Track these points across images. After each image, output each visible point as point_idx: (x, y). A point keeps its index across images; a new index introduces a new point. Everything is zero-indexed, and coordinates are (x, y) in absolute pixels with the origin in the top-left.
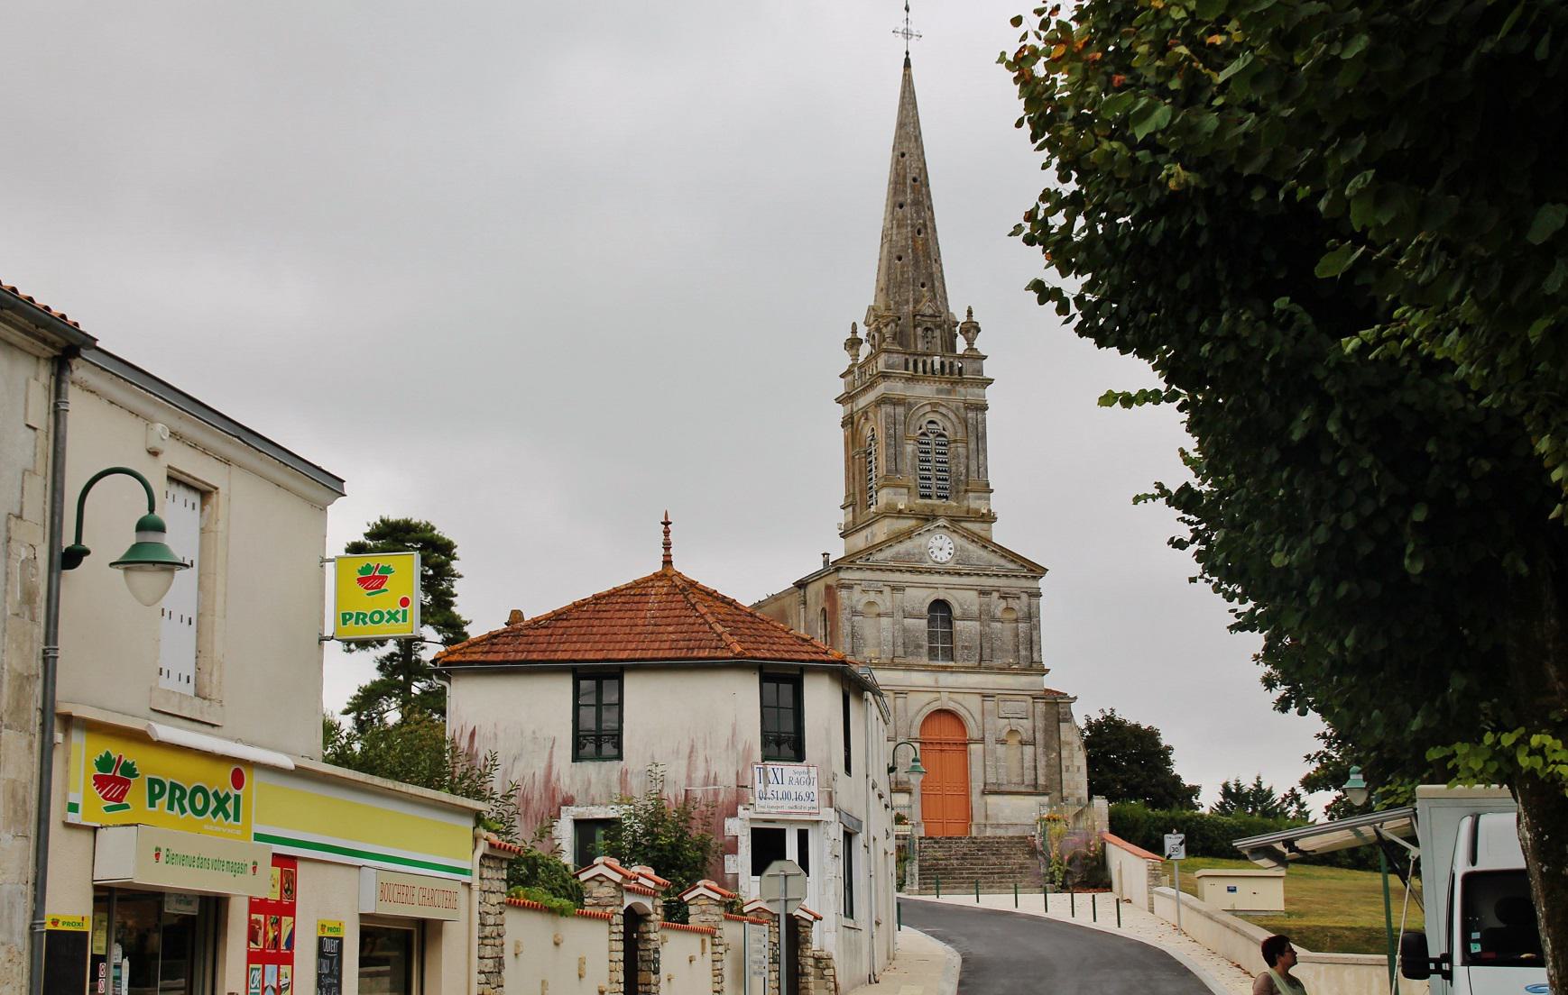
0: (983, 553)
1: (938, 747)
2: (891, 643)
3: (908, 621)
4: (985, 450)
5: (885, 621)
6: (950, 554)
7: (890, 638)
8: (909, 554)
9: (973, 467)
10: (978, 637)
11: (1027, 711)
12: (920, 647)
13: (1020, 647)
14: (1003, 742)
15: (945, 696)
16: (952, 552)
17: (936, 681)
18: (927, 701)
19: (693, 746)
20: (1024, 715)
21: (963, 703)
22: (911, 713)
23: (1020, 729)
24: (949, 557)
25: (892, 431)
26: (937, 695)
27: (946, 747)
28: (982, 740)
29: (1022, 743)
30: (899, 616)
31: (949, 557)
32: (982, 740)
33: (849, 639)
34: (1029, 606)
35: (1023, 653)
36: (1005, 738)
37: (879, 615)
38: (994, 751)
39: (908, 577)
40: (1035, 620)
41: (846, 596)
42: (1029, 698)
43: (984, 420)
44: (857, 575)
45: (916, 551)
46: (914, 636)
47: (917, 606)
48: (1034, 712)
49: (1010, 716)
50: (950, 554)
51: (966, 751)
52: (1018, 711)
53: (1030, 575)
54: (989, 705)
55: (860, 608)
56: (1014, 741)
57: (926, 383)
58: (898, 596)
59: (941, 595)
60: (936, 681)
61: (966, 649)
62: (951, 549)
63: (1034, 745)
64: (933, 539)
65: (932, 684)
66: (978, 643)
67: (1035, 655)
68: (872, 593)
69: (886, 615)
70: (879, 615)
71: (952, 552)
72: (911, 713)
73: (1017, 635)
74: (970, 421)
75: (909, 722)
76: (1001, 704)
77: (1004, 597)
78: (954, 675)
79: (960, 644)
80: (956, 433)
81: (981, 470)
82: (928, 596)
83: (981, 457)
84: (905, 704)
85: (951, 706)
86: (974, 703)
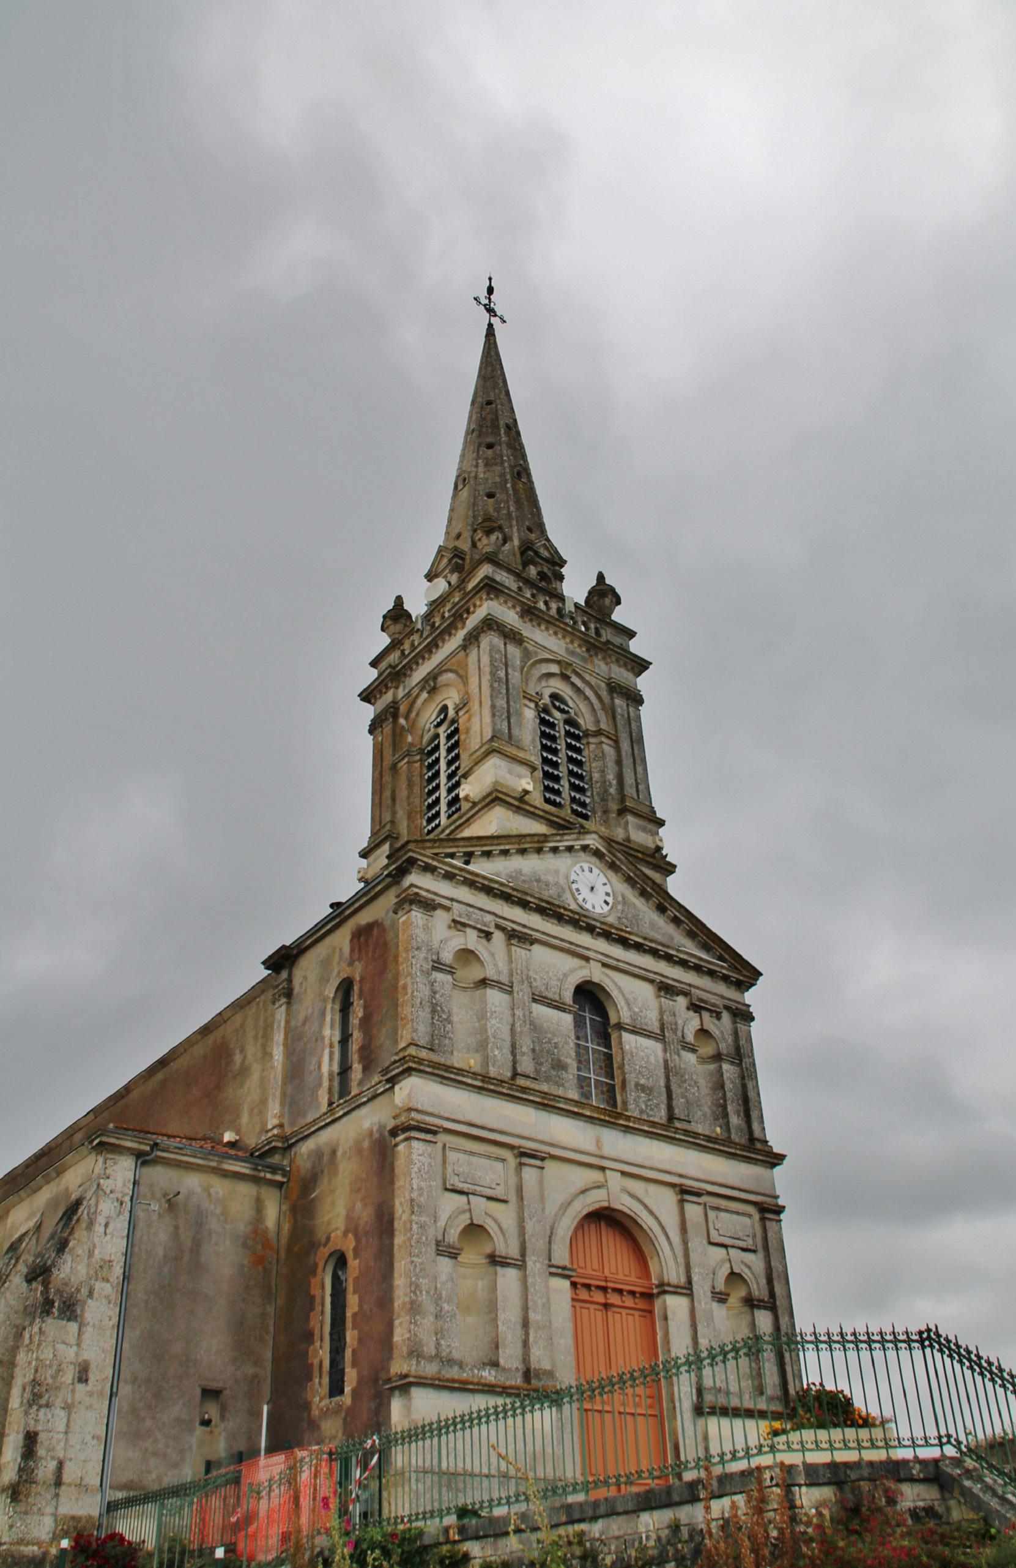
0: (660, 921)
1: (599, 1297)
2: (508, 1044)
3: (539, 1010)
4: (644, 760)
5: (494, 997)
6: (606, 903)
7: (506, 1035)
8: (538, 880)
9: (629, 780)
10: (661, 1073)
11: (754, 1236)
12: (564, 1067)
13: (729, 1108)
14: (453, 1254)
15: (615, 1180)
16: (610, 900)
17: (598, 1142)
18: (580, 1185)
19: (523, 749)
20: (749, 1243)
21: (647, 1201)
22: (551, 1208)
23: (747, 1274)
24: (606, 908)
25: (502, 674)
26: (597, 1176)
27: (614, 1299)
28: (687, 1289)
29: (495, 1260)
30: (522, 993)
31: (606, 908)
32: (687, 1289)
33: (425, 1014)
34: (736, 1034)
35: (735, 1120)
36: (723, 1289)
37: (483, 983)
38: (710, 1318)
39: (535, 921)
40: (746, 1060)
41: (420, 923)
42: (751, 1210)
43: (639, 717)
44: (445, 889)
45: (550, 879)
46: (549, 1042)
47: (554, 983)
48: (730, 1237)
49: (727, 1241)
50: (606, 903)
51: (651, 1312)
52: (741, 1235)
53: (735, 975)
54: (693, 1211)
55: (447, 956)
56: (472, 1256)
57: (543, 627)
58: (519, 952)
59: (597, 974)
60: (598, 1142)
61: (643, 1091)
62: (608, 894)
63: (690, 1295)
64: (577, 868)
65: (591, 1147)
66: (662, 1083)
67: (755, 1126)
68: (472, 934)
69: (498, 985)
70: (483, 983)
71: (610, 900)
72: (551, 1208)
73: (722, 1086)
74: (619, 710)
75: (548, 1228)
76: (711, 1214)
77: (696, 1007)
78: (630, 1137)
79: (631, 1078)
80: (598, 722)
81: (640, 787)
82: (575, 972)
83: (639, 769)
84: (541, 1182)
85: (624, 1204)
86: (664, 1202)
